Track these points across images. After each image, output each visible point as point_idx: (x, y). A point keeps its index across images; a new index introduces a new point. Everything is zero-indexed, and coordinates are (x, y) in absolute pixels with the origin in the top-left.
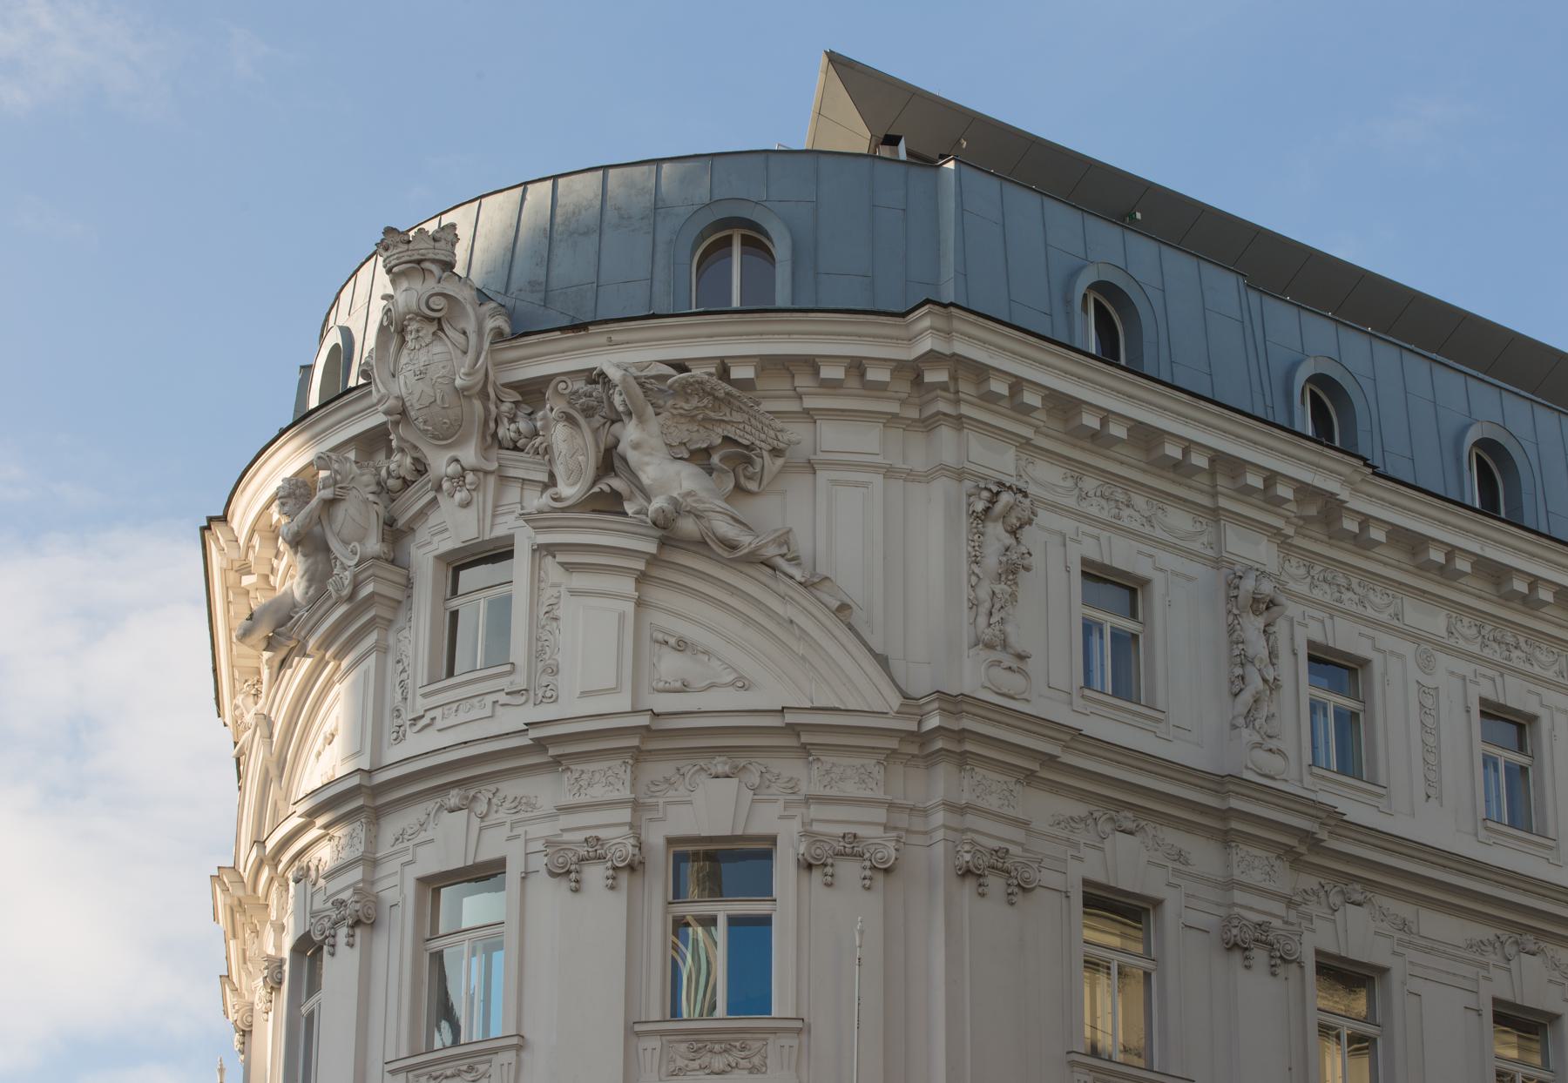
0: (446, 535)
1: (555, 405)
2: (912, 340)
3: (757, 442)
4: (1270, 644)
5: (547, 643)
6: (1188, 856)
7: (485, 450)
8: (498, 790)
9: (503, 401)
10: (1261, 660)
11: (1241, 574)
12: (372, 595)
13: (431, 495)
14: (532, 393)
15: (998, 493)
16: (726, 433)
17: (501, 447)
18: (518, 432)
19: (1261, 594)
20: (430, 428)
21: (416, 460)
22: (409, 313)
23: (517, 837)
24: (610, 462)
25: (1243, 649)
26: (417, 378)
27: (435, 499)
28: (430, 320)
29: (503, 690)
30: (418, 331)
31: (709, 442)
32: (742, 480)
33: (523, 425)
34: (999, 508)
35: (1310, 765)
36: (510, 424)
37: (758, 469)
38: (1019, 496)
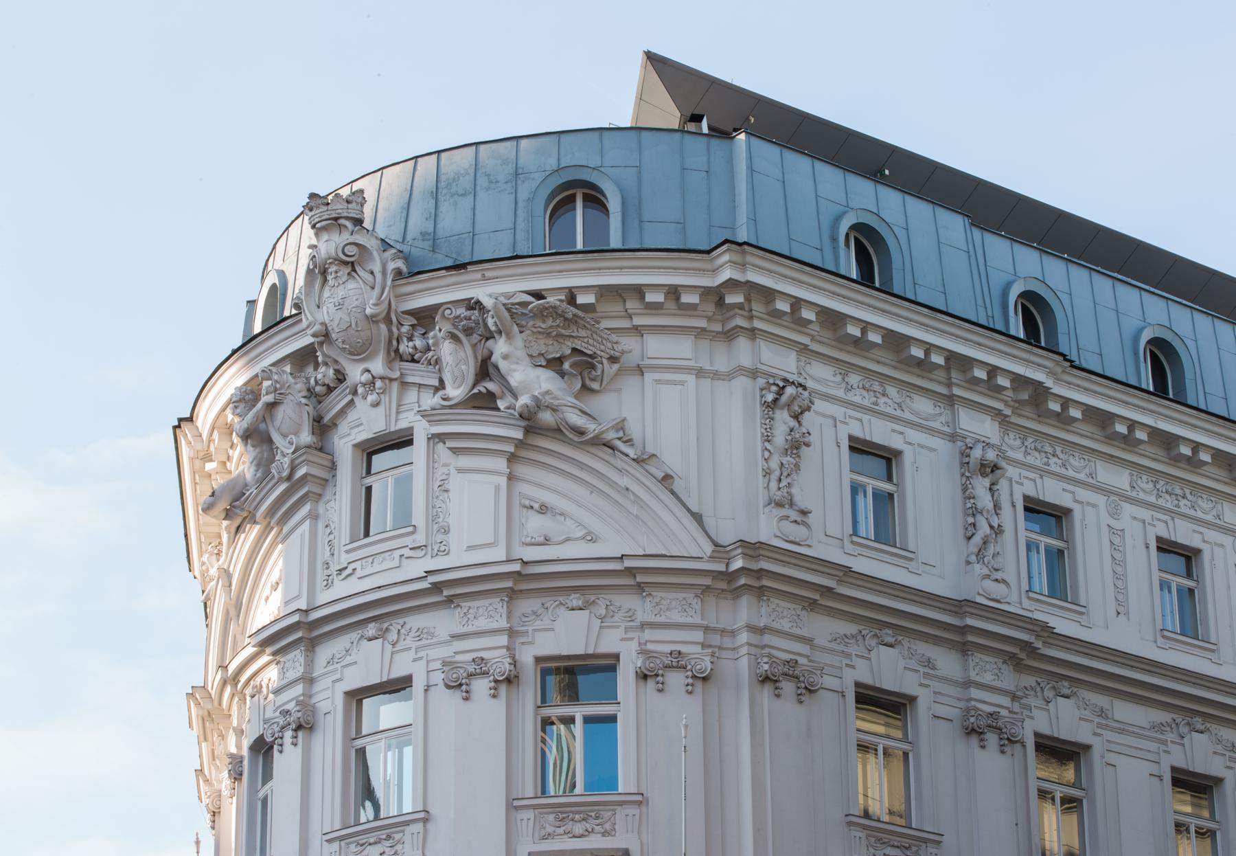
0: (361, 428)
1: (442, 327)
2: (715, 271)
3: (598, 352)
4: (995, 499)
5: (440, 510)
6: (935, 662)
7: (390, 362)
8: (405, 623)
9: (402, 325)
10: (988, 511)
11: (970, 445)
12: (305, 476)
13: (349, 398)
14: (425, 318)
15: (784, 387)
16: (574, 346)
17: (402, 360)
18: (415, 348)
19: (986, 460)
20: (347, 347)
21: (337, 371)
22: (329, 259)
23: (421, 658)
24: (485, 369)
25: (974, 503)
26: (336, 308)
27: (352, 401)
28: (346, 263)
29: (407, 546)
30: (336, 272)
31: (561, 353)
32: (588, 382)
33: (418, 342)
34: (784, 398)
35: (1027, 591)
36: (408, 342)
37: (599, 373)
38: (800, 390)
